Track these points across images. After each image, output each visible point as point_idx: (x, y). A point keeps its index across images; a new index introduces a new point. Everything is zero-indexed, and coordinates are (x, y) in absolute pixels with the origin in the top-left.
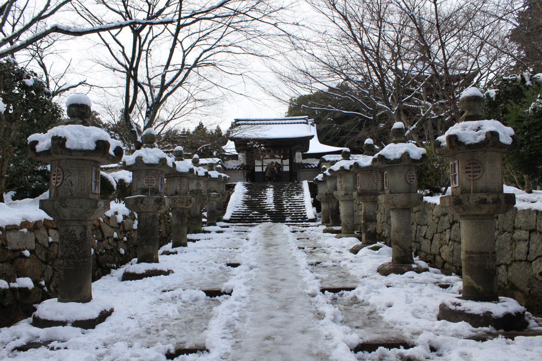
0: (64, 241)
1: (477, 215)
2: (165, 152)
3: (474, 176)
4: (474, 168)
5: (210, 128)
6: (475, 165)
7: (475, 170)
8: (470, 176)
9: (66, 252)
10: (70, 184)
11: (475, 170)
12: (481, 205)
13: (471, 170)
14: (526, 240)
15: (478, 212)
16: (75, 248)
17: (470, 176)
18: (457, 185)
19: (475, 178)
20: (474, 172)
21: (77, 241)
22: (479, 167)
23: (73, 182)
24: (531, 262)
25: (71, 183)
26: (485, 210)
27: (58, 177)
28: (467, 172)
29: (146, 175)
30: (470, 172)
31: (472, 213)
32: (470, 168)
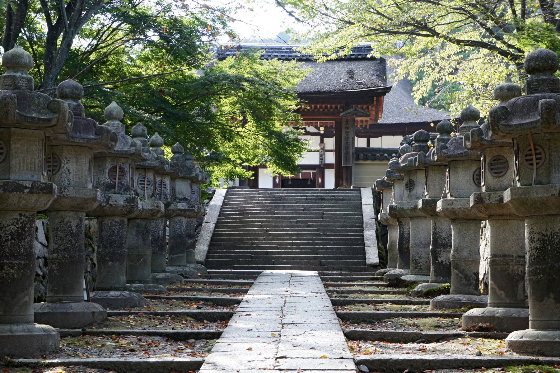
0: (59, 233)
9: (60, 245)
10: (67, 172)
16: (71, 241)
21: (73, 233)
23: (71, 171)
25: (69, 170)
27: (55, 164)
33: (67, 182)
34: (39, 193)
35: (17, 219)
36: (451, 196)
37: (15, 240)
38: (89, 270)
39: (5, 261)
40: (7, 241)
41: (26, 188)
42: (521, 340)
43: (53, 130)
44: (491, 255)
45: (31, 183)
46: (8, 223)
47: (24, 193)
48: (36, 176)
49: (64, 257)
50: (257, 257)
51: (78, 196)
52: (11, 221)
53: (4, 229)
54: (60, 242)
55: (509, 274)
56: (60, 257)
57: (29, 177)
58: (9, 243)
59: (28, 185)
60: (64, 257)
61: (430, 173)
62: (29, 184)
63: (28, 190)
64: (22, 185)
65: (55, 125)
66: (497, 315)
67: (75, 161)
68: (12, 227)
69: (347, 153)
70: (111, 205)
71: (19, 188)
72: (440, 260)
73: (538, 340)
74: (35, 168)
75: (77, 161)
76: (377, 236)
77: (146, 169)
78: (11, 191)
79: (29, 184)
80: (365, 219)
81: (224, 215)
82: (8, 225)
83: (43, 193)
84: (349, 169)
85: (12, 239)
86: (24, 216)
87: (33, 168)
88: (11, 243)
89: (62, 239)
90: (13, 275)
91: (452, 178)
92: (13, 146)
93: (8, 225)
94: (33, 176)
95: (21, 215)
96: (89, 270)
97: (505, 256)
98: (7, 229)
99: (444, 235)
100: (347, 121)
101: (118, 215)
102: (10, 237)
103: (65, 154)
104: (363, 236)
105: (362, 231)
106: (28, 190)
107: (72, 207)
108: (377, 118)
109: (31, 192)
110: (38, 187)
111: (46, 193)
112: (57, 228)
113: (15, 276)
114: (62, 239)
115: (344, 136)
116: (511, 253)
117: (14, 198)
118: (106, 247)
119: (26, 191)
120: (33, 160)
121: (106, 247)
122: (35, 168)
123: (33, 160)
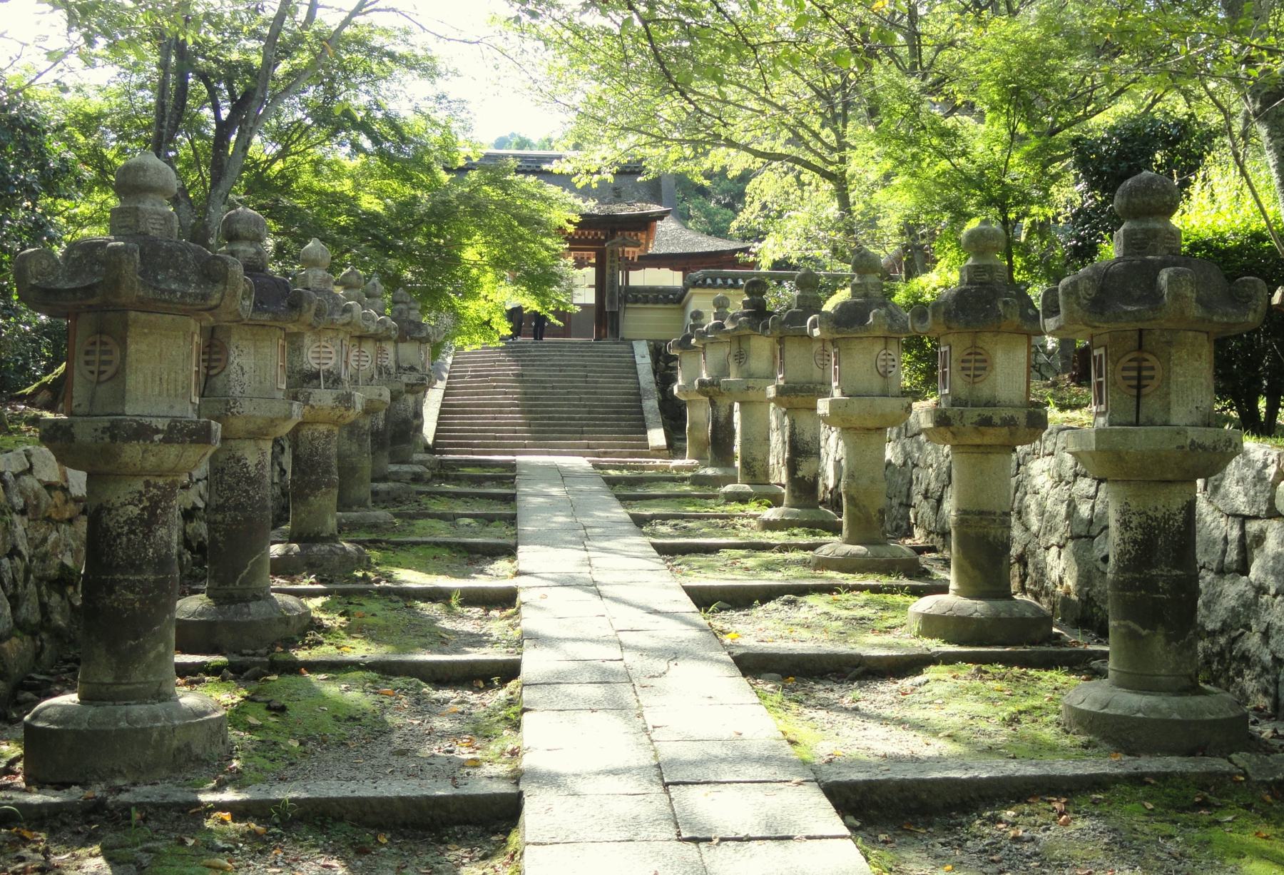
1: (979, 446)
2: (753, 665)
3: (975, 376)
4: (976, 361)
5: (565, 172)
6: (978, 357)
7: (978, 365)
8: (92, 372)
11: (978, 365)
12: (982, 428)
13: (972, 365)
14: (1091, 498)
15: (978, 441)
16: (246, 491)
17: (92, 372)
18: (947, 391)
19: (977, 380)
20: (976, 369)
21: (250, 478)
22: (985, 361)
23: (246, 368)
24: (1093, 538)
26: (991, 436)
28: (963, 369)
29: (313, 341)
30: (969, 369)
31: (969, 442)
32: (970, 361)
33: (239, 389)
34: (183, 442)
35: (140, 492)
36: (843, 394)
37: (135, 534)
38: (276, 480)
39: (119, 576)
40: (119, 535)
41: (157, 431)
42: (1106, 711)
43: (212, 315)
44: (958, 510)
45: (167, 421)
46: (122, 500)
47: (152, 441)
48: (178, 407)
49: (234, 519)
50: (502, 438)
51: (258, 414)
52: (128, 497)
53: (114, 512)
54: (227, 493)
55: (989, 543)
56: (228, 519)
57: (163, 409)
58: (125, 539)
59: (160, 427)
60: (234, 519)
61: (788, 345)
62: (162, 424)
63: (161, 436)
64: (149, 426)
65: (216, 307)
66: (975, 615)
67: (252, 351)
68: (131, 508)
69: (612, 294)
70: (312, 407)
71: (142, 432)
72: (800, 474)
73: (1140, 715)
74: (176, 390)
75: (256, 351)
76: (660, 408)
77: (361, 338)
78: (128, 439)
79: (162, 424)
80: (642, 384)
81: (455, 377)
82: (123, 505)
83: (192, 442)
84: (615, 316)
85: (132, 532)
86: (155, 486)
87: (172, 392)
88: (129, 540)
89: (231, 488)
90: (132, 604)
91: (843, 364)
92: (132, 348)
93: (123, 505)
94: (172, 407)
95: (147, 484)
96: (276, 480)
97: (981, 513)
98: (120, 512)
99: (807, 437)
100: (612, 252)
101: (458, 823)
102: (126, 528)
103: (234, 339)
104: (641, 407)
105: (640, 401)
106: (161, 436)
107: (249, 432)
108: (647, 248)
109: (168, 440)
110: (182, 429)
111: (197, 442)
112: (223, 469)
113: (137, 605)
114: (231, 488)
115: (608, 271)
116: (992, 509)
117: (132, 452)
118: (304, 472)
119: (157, 437)
120: (173, 375)
121: (304, 472)
122: (176, 390)
123: (173, 375)
